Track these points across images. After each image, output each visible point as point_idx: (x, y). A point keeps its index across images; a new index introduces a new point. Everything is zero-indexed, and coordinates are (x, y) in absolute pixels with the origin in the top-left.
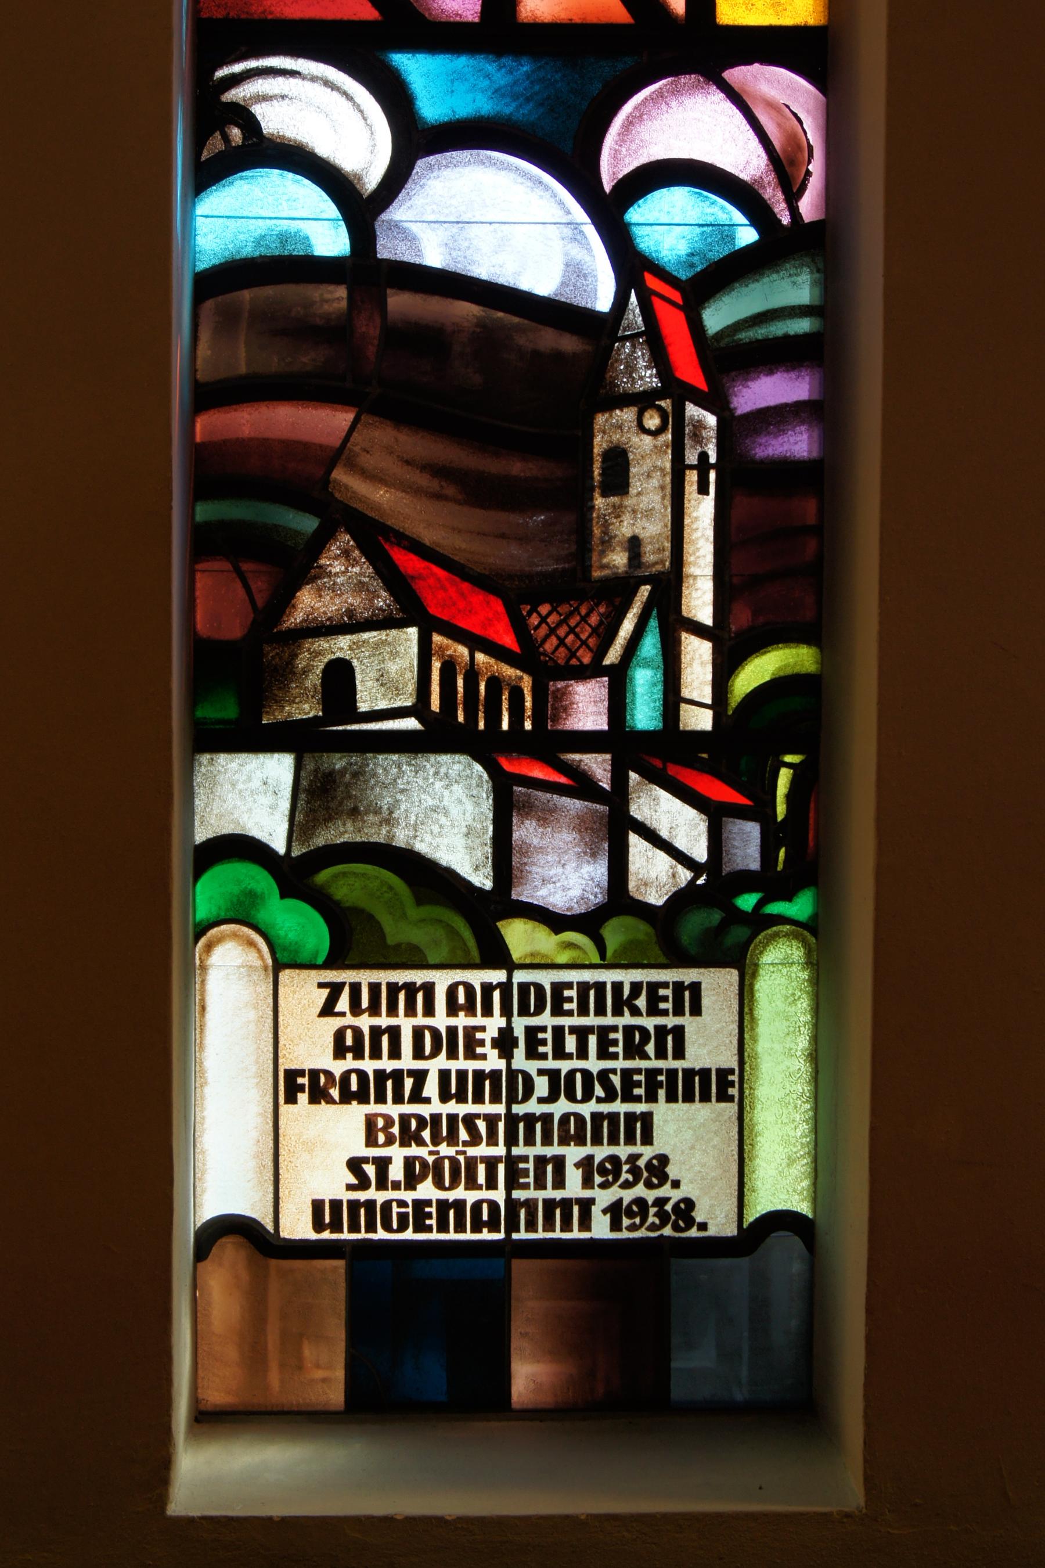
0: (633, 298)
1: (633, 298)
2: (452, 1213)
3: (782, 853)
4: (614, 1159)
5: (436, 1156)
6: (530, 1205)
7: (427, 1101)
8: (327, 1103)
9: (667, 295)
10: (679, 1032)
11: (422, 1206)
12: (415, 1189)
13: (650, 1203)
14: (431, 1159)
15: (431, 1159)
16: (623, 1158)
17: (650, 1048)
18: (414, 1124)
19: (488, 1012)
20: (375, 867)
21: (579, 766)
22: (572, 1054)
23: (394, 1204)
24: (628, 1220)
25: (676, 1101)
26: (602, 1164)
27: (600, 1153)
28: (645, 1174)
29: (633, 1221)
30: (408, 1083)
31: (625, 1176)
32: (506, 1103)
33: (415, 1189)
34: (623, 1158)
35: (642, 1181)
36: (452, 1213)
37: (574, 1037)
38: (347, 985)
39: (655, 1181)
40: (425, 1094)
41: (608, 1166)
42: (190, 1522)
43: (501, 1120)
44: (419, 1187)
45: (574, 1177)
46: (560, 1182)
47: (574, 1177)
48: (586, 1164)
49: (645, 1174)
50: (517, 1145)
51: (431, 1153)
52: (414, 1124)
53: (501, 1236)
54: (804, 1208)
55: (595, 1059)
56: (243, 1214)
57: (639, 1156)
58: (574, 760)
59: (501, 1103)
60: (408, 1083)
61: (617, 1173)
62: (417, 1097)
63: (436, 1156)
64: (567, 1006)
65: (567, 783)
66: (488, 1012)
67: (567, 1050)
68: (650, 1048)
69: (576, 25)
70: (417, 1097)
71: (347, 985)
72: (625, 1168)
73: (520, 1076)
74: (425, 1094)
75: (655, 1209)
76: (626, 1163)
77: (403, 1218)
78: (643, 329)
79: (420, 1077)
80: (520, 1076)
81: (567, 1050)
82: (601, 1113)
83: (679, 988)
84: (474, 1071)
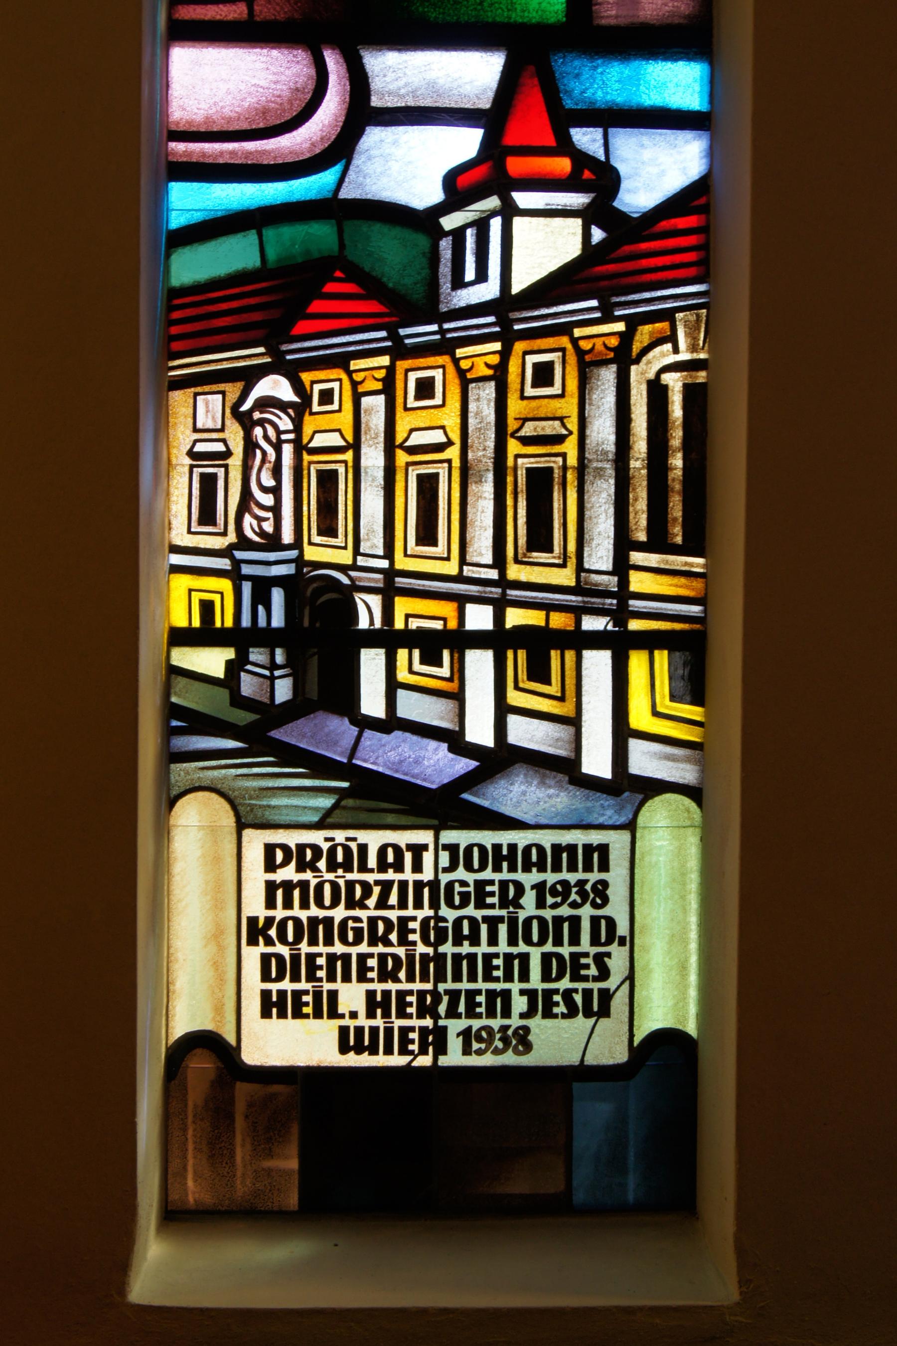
0: (696, 203)
1: (696, 203)
4: (565, 883)
5: (332, 843)
9: (567, 687)
14: (325, 846)
15: (325, 846)
16: (496, 1029)
18: (309, 854)
19: (418, 905)
21: (612, 460)
27: (551, 878)
28: (592, 896)
31: (574, 897)
34: (496, 1029)
35: (589, 901)
37: (459, 1011)
39: (599, 901)
41: (559, 887)
49: (592, 896)
51: (327, 840)
52: (309, 854)
57: (586, 881)
59: (442, 845)
61: (490, 1041)
63: (332, 843)
64: (489, 900)
66: (418, 905)
72: (574, 890)
76: (498, 1032)
78: (669, 333)
82: (511, 954)
83: (589, 849)
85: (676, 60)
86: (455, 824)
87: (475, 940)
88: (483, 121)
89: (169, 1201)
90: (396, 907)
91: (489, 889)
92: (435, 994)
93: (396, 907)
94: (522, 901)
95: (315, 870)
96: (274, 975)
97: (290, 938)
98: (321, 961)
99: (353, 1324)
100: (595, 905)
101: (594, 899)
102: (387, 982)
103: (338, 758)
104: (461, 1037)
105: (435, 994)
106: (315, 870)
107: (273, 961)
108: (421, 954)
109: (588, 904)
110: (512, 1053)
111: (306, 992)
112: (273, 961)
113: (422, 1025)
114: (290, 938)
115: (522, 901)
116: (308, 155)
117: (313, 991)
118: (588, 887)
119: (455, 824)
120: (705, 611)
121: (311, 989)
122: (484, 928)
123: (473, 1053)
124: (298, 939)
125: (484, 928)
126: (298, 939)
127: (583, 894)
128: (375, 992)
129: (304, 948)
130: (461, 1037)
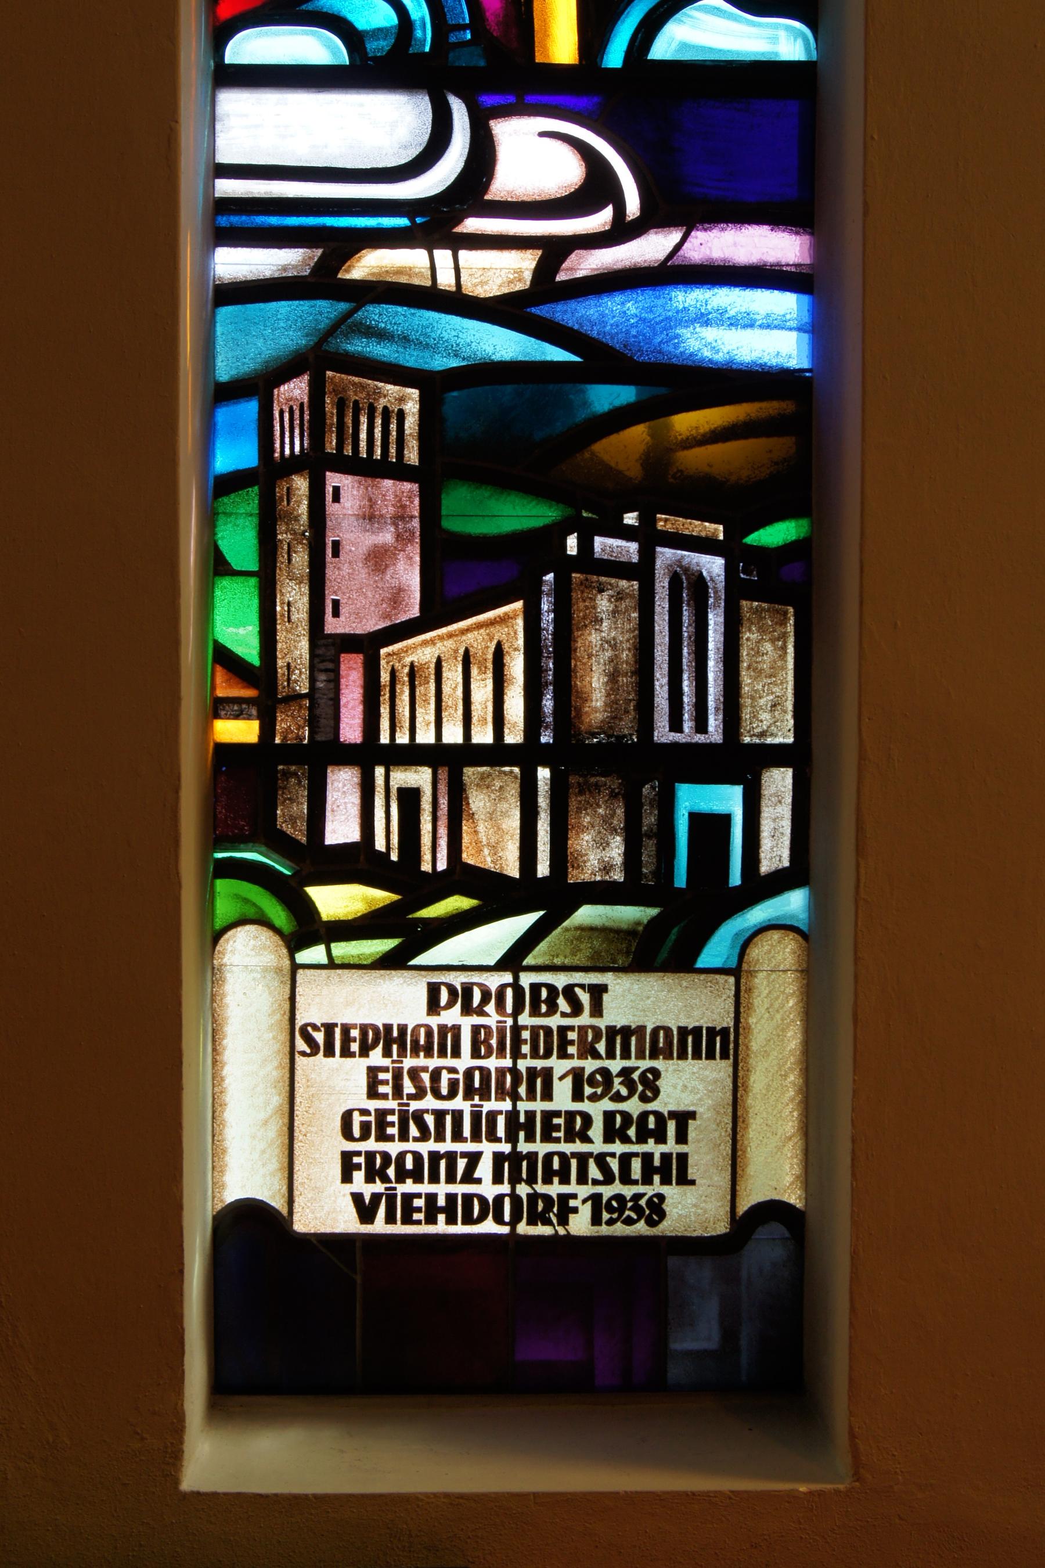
6: (501, 1095)
7: (479, 1181)
11: (435, 1212)
12: (367, 1056)
13: (614, 1074)
20: (388, 730)
23: (356, 1114)
24: (590, 1089)
25: (700, 1058)
26: (592, 1075)
27: (590, 1065)
29: (594, 1090)
30: (462, 1164)
32: (324, 544)
33: (367, 1056)
40: (476, 1175)
42: (197, 1495)
44: (371, 1053)
45: (563, 1090)
46: (548, 1095)
47: (563, 1090)
48: (578, 1076)
49: (640, 1088)
53: (505, 1230)
54: (794, 1198)
55: (674, 1142)
60: (462, 1164)
62: (469, 1177)
70: (469, 1177)
74: (476, 1175)
75: (621, 1079)
77: (365, 1127)
79: (474, 1158)
84: (534, 1141)
88: (254, 712)
91: (556, 1121)
92: (514, 1071)
94: (590, 1133)
97: (507, 1218)
99: (875, 1460)
100: (644, 1099)
101: (643, 1092)
104: (589, 1203)
105: (514, 1071)
107: (476, 1202)
110: (637, 1099)
111: (392, 1112)
112: (476, 1202)
114: (507, 1218)
115: (590, 1133)
117: (399, 1110)
118: (636, 1076)
121: (397, 1108)
122: (574, 1163)
123: (586, 1100)
125: (574, 1163)
127: (631, 1085)
129: (525, 1019)
130: (589, 1203)
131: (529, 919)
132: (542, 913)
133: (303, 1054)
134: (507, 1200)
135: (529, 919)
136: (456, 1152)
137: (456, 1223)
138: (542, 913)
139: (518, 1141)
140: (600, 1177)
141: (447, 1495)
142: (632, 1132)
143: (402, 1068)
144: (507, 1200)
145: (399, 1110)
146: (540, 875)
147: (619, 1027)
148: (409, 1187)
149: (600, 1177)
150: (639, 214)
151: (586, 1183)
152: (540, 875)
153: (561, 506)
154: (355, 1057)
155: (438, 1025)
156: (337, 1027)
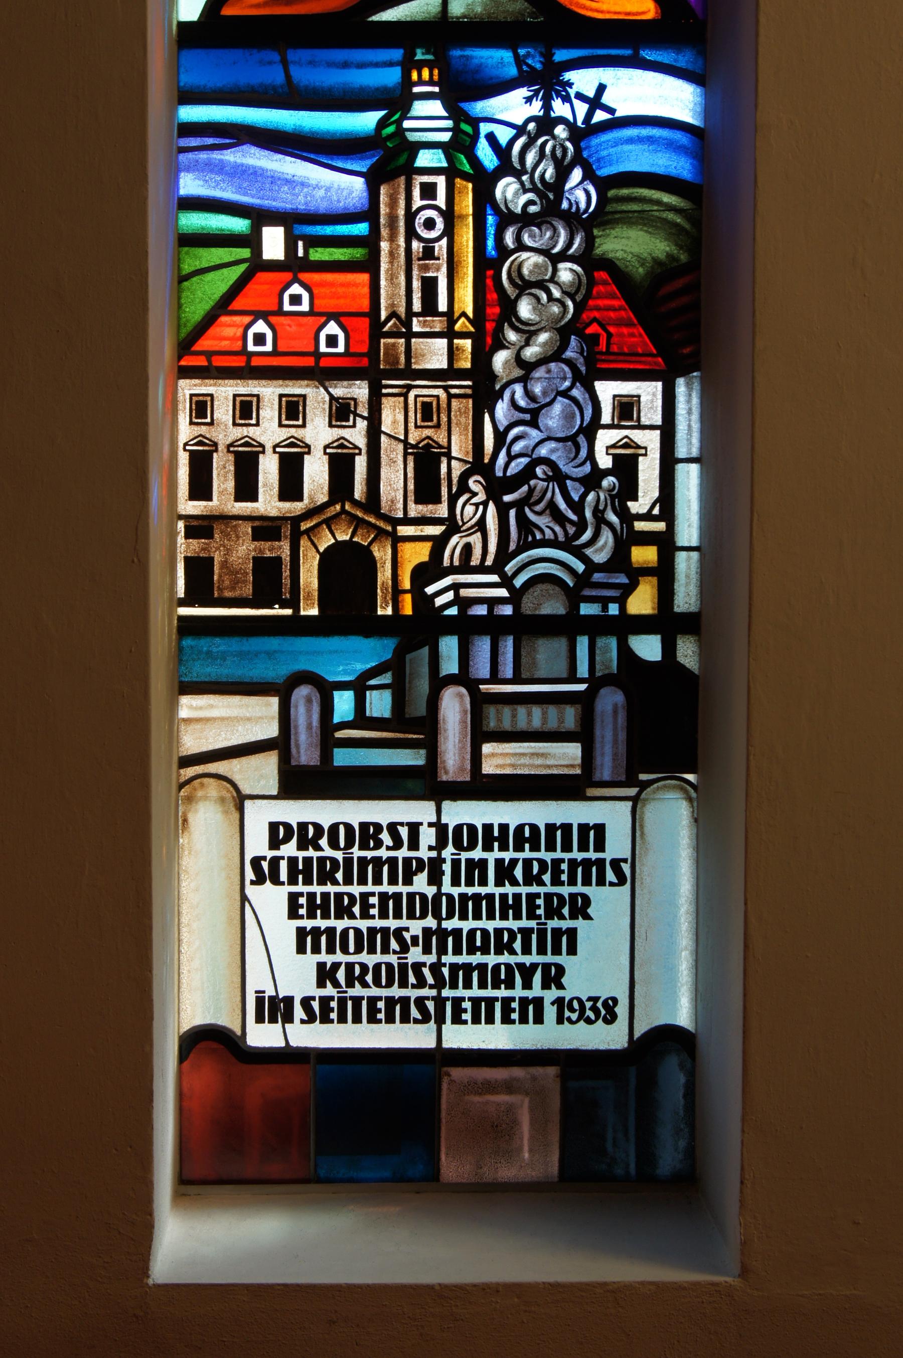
2: (594, 869)
3: (282, 1004)
8: (584, 919)
10: (572, 934)
17: (517, 945)
22: (303, 915)
36: (594, 869)
38: (343, 964)
43: (364, 1000)
50: (446, 953)
56: (202, 1023)
58: (571, 157)
65: (486, 452)
67: (282, 880)
68: (517, 945)
69: (403, 22)
71: (343, 964)
73: (555, 898)
80: (555, 898)
81: (282, 880)
85: (297, 1047)
86: (228, 141)
87: (510, 985)
89: (215, 418)
90: (286, 883)
93: (286, 883)
95: (318, 848)
96: (418, 915)
98: (374, 900)
102: (326, 884)
103: (301, 581)
106: (318, 848)
108: (553, 929)
109: (600, 1021)
113: (322, 995)
116: (291, 131)
119: (228, 141)
120: (173, 113)
124: (350, 844)
126: (350, 844)
128: (304, 883)
129: (356, 852)
131: (584, 425)
132: (328, 969)
133: (625, 861)
134: (444, 916)
135: (584, 425)
136: (568, 885)
137: (461, 954)
138: (328, 969)
139: (445, 1023)
140: (615, 880)
141: (604, 1284)
142: (566, 911)
143: (408, 963)
144: (444, 916)
145: (338, 997)
146: (426, 590)
147: (460, 963)
148: (357, 991)
149: (615, 880)
150: (310, 686)
151: (604, 885)
152: (426, 590)
153: (690, 203)
154: (564, 885)
155: (354, 987)
156: (334, 1000)
